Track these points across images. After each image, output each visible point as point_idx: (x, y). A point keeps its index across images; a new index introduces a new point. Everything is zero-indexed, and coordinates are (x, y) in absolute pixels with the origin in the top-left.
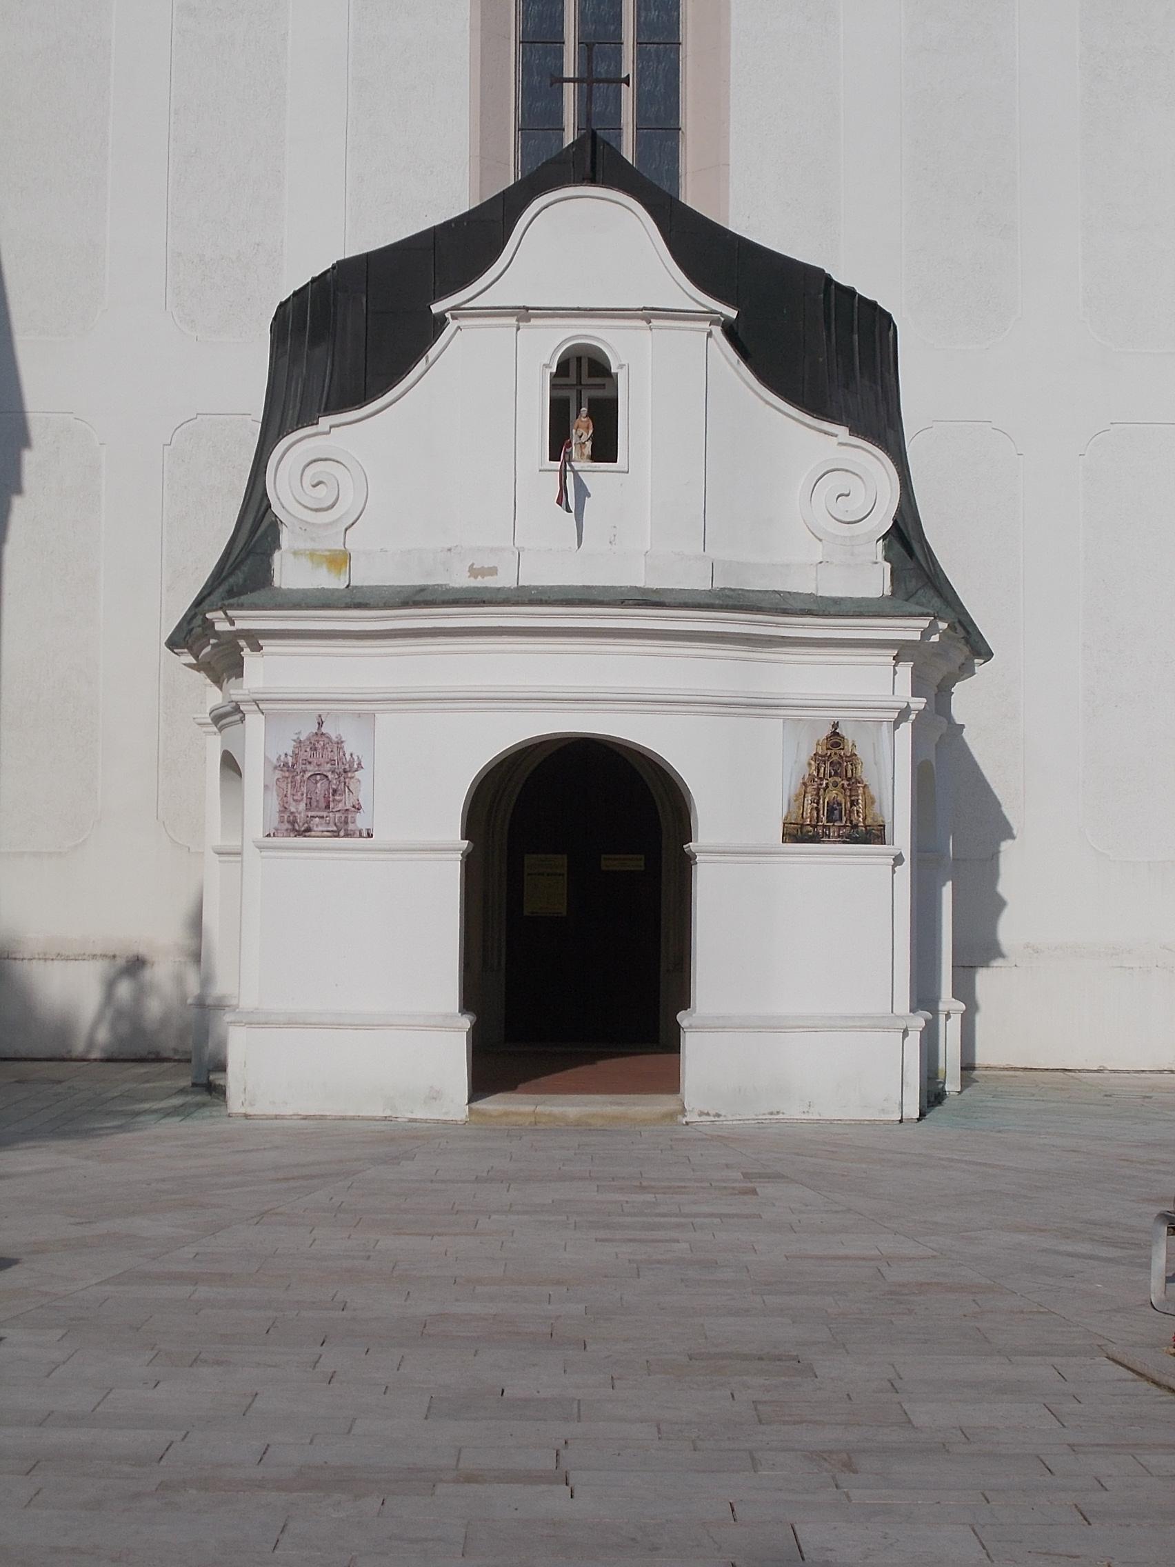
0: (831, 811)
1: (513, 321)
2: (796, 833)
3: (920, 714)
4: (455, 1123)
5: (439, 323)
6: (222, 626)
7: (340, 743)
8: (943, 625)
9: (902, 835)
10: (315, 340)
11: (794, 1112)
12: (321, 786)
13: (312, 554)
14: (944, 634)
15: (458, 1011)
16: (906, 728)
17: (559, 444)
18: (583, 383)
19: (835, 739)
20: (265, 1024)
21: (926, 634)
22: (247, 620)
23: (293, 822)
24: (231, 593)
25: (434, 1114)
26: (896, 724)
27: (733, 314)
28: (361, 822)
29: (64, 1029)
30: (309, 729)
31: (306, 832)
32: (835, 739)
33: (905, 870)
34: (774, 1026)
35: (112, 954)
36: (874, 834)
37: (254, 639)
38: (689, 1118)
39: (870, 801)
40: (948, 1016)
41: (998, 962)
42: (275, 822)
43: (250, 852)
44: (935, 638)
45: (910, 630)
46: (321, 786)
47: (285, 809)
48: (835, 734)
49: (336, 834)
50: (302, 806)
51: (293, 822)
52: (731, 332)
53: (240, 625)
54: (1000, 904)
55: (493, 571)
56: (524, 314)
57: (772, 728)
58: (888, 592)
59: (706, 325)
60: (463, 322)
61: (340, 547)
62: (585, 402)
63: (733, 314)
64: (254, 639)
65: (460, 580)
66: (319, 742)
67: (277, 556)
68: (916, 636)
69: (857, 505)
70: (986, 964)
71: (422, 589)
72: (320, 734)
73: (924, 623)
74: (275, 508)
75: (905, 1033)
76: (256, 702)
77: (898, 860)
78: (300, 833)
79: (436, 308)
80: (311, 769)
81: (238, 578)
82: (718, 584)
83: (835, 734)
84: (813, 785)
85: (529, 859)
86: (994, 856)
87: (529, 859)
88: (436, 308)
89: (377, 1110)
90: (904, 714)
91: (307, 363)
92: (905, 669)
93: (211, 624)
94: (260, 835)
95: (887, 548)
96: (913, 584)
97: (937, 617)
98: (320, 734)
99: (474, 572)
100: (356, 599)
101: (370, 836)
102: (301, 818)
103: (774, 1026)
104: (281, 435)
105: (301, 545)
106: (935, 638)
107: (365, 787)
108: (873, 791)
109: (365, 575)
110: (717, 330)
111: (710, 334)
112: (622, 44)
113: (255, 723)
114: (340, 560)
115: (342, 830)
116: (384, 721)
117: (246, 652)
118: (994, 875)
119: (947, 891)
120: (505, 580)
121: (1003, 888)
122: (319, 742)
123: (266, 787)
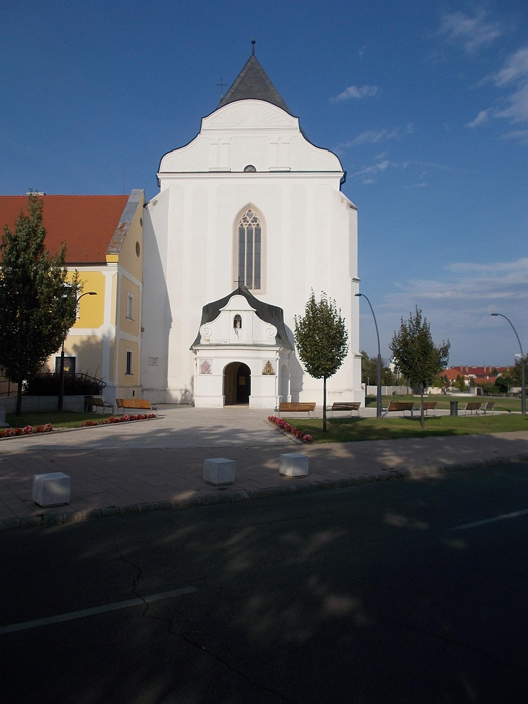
0: (268, 371)
1: (229, 311)
2: (264, 374)
3: (280, 359)
4: (221, 409)
5: (221, 311)
6: (194, 348)
7: (208, 363)
8: (282, 348)
9: (277, 374)
10: (207, 313)
11: (263, 408)
12: (206, 368)
13: (205, 340)
14: (282, 349)
15: (222, 395)
16: (278, 361)
17: (235, 326)
18: (112, 413)
19: (269, 362)
20: (199, 397)
21: (280, 349)
22: (197, 348)
23: (203, 372)
24: (195, 345)
25: (219, 407)
26: (276, 360)
27: (256, 310)
28: (211, 372)
29: (176, 400)
30: (205, 361)
31: (204, 373)
32: (269, 362)
33: (277, 378)
34: (261, 397)
35: (180, 389)
36: (273, 374)
37: (198, 350)
38: (250, 408)
39: (273, 370)
40: (289, 397)
41: (302, 391)
42: (201, 372)
43: (198, 376)
44: (281, 350)
45: (278, 349)
46: (206, 368)
47: (202, 371)
48: (269, 362)
49: (208, 374)
50: (204, 370)
51: (203, 372)
52: (256, 312)
53: (196, 348)
54: (303, 383)
55: (226, 342)
56: (230, 311)
57: (261, 361)
58: (275, 344)
59: (253, 312)
60: (223, 312)
61: (208, 339)
62: (239, 321)
63: (256, 310)
64: (198, 350)
65: (223, 343)
66: (206, 362)
67: (201, 340)
68: (278, 349)
69: (272, 333)
70: (300, 392)
71: (218, 344)
72: (206, 362)
73: (279, 348)
74: (201, 334)
75: (277, 398)
76: (198, 358)
77: (276, 377)
78: (203, 374)
79: (220, 310)
80: (205, 366)
81: (196, 343)
82: (254, 343)
83: (269, 362)
84: (266, 368)
85: (240, 378)
86: (302, 377)
87: (240, 378)
88: (220, 310)
89: (212, 407)
90: (277, 359)
91: (115, 447)
92: (278, 353)
93: (193, 348)
94: (199, 374)
95: (276, 338)
96: (278, 343)
97: (281, 347)
98: (206, 362)
99: (224, 342)
100: (210, 345)
101: (212, 374)
102: (204, 372)
103: (261, 397)
104: (203, 324)
105: (204, 338)
106: (281, 350)
107: (211, 368)
108: (273, 369)
109: (211, 342)
110: (254, 312)
111: (253, 313)
112: (260, 254)
113: (198, 360)
114: (208, 340)
115: (209, 373)
116: (214, 360)
117: (197, 351)
118: (302, 379)
119: (289, 381)
120: (228, 343)
121: (303, 381)
122: (206, 362)
123: (200, 368)
